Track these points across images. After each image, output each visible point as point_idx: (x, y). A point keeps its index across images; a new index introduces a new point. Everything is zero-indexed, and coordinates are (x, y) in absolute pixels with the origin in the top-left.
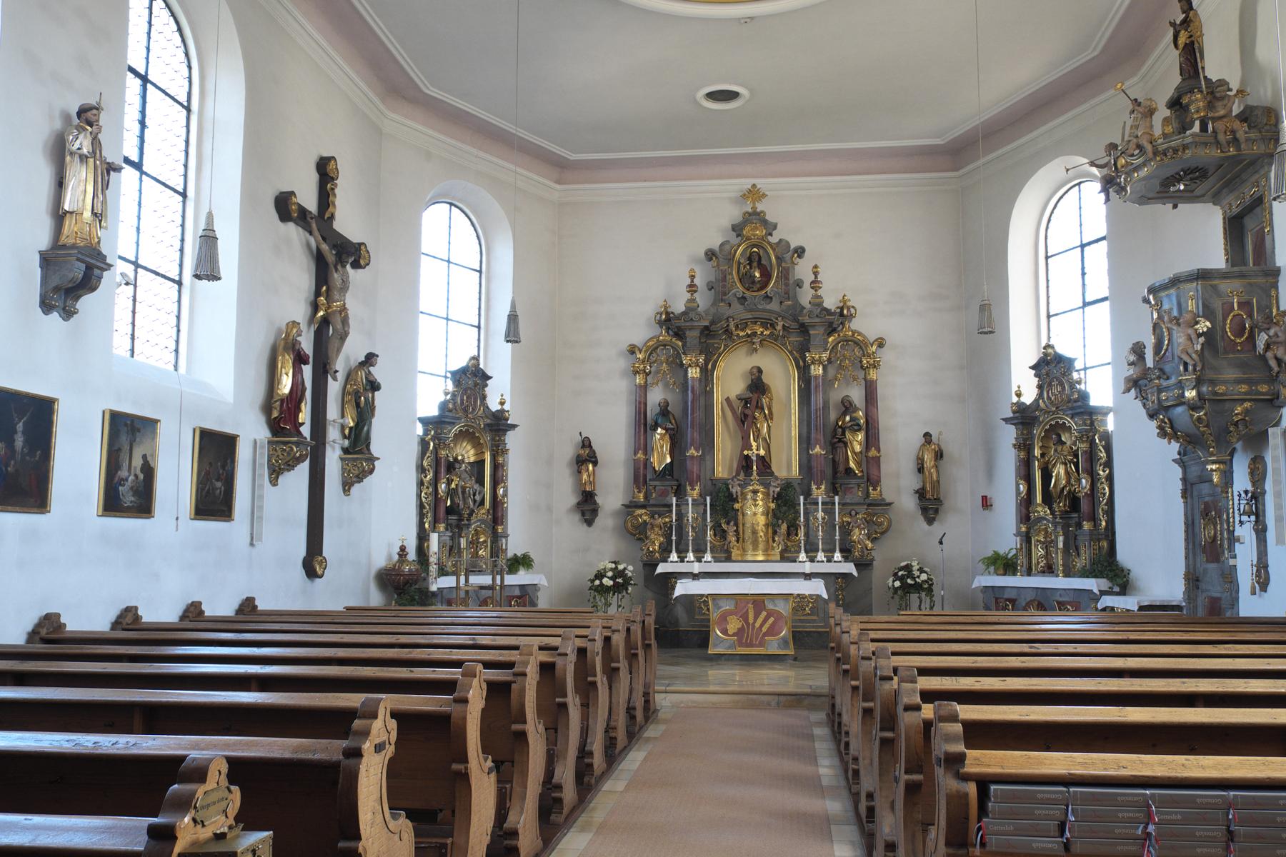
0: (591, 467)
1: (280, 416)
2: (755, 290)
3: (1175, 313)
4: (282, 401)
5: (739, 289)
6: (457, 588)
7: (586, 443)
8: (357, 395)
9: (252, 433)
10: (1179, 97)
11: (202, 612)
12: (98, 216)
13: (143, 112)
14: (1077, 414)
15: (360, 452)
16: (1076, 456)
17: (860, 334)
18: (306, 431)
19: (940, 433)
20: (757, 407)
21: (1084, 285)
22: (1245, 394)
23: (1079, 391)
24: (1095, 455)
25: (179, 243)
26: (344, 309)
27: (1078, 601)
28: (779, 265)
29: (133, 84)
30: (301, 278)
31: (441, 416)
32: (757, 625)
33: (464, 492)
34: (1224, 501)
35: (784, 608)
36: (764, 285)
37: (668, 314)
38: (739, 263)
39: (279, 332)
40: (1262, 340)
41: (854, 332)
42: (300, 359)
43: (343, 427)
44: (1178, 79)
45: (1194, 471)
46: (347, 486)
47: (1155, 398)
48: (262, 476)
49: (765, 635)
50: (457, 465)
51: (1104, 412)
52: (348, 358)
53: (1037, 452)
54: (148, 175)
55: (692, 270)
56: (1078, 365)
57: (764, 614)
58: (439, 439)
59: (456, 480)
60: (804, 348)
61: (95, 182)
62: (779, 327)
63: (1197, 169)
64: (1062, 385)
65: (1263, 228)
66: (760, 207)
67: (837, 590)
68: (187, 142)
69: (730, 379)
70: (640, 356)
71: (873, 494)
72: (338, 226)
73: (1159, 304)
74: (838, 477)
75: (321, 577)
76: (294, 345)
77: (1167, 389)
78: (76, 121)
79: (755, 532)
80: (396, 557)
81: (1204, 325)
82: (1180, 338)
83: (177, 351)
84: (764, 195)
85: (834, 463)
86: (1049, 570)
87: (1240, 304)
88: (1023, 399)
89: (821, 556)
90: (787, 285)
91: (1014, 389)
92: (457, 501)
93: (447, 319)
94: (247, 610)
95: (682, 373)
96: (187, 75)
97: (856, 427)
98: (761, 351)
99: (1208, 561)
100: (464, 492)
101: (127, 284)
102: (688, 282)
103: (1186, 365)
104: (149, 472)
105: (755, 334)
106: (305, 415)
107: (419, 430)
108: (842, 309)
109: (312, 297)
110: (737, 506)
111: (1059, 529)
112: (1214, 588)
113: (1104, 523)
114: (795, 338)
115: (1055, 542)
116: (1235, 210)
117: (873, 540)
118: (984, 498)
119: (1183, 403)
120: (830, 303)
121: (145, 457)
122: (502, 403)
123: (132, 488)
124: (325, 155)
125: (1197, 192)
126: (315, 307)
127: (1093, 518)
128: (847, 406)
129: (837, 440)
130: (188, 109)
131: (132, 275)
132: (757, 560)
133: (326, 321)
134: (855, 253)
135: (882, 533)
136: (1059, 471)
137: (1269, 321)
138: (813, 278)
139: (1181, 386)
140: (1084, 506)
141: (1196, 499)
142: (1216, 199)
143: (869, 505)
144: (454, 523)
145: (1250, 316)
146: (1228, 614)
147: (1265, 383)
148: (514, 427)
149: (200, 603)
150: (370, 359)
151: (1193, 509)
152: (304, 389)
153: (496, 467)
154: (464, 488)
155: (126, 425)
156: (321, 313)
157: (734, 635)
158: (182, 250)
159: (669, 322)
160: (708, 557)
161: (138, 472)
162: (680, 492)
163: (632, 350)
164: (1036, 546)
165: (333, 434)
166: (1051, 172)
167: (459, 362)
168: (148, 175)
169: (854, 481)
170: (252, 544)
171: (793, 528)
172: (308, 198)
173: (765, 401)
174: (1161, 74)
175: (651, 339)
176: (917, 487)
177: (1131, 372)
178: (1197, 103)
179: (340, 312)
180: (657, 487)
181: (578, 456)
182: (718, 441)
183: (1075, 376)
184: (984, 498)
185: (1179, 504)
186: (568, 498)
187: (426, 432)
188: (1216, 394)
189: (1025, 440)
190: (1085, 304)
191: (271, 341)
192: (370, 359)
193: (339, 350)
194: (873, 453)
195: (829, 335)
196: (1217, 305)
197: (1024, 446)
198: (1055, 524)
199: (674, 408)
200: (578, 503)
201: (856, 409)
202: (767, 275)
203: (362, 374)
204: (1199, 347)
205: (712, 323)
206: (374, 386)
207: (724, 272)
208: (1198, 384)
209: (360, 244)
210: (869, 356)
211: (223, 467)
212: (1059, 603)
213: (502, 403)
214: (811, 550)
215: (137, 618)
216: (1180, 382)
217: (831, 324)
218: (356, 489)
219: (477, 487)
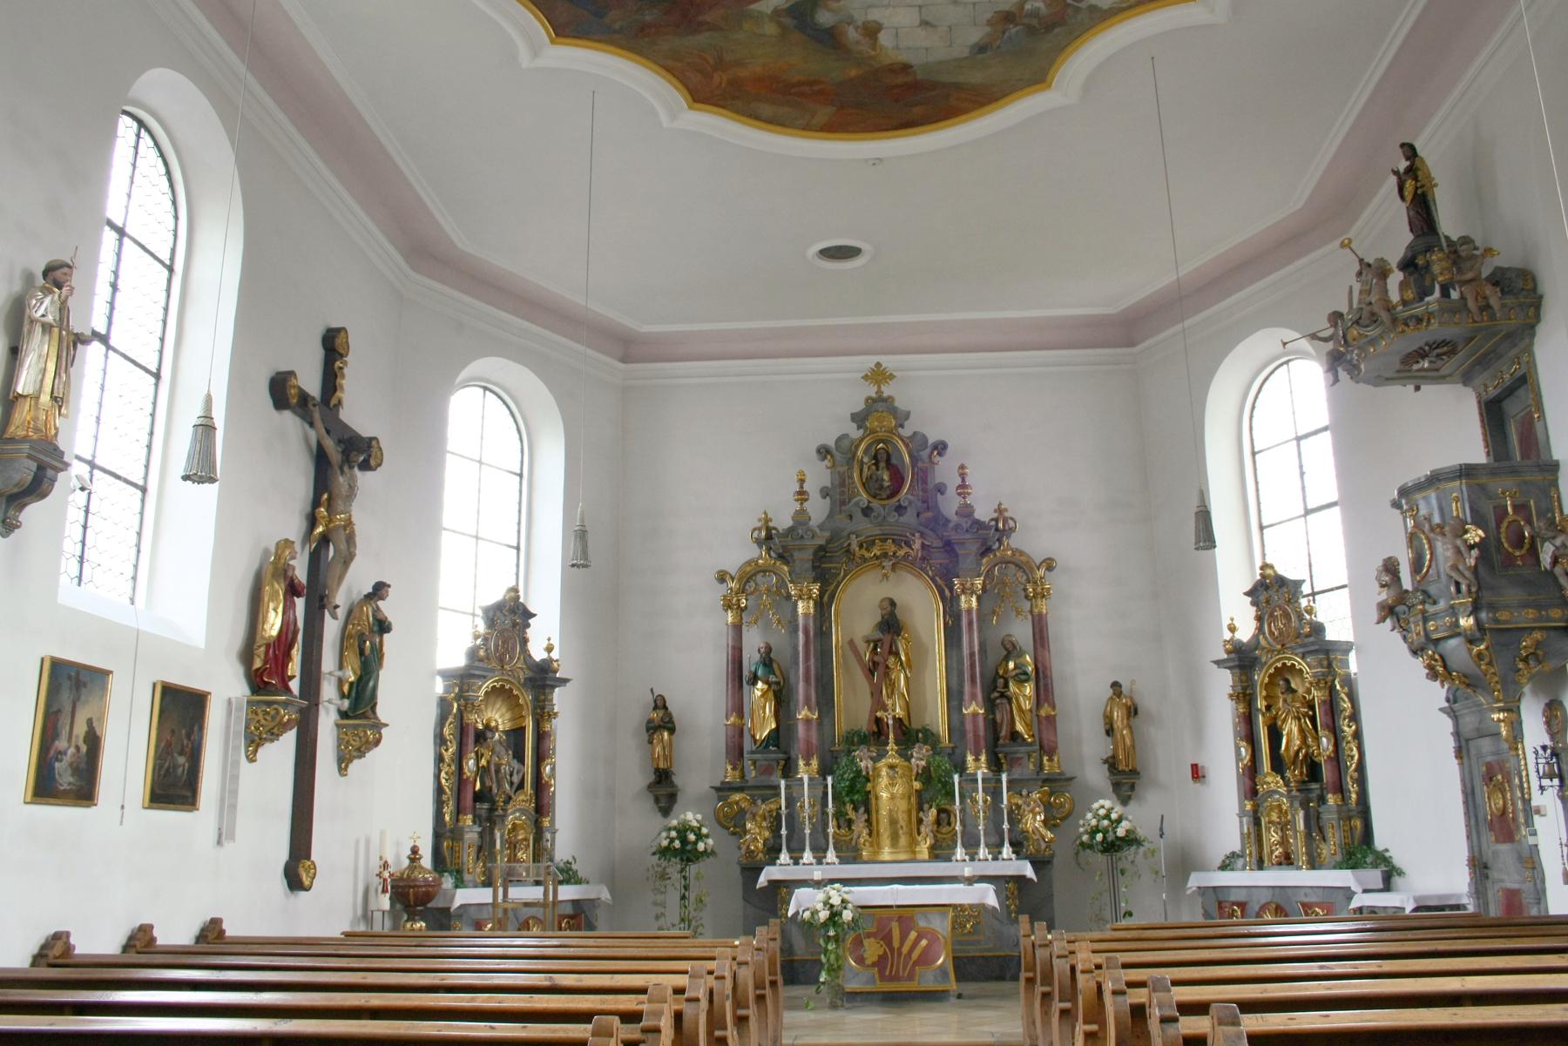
1: (265, 669)
3: (1437, 519)
4: (268, 646)
6: (494, 904)
7: (660, 704)
8: (362, 639)
9: (226, 688)
10: (1414, 257)
11: (153, 939)
12: (58, 400)
13: (116, 273)
14: (1310, 652)
15: (364, 716)
16: (1312, 708)
17: (1022, 553)
18: (294, 685)
19: (1133, 682)
21: (1303, 488)
22: (1534, 620)
23: (1311, 623)
24: (1335, 708)
25: (147, 437)
26: (349, 523)
27: (1328, 904)
29: (109, 237)
30: (300, 483)
31: (469, 667)
32: (905, 950)
34: (1513, 761)
35: (942, 926)
37: (769, 530)
39: (266, 552)
40: (1546, 558)
41: (1015, 551)
42: (293, 590)
43: (340, 682)
44: (1409, 237)
45: (1469, 722)
46: (343, 762)
47: (1420, 628)
48: (236, 748)
49: (915, 964)
50: (489, 734)
51: (1346, 648)
52: (349, 591)
53: (1261, 704)
54: (115, 351)
55: (802, 473)
56: (1306, 589)
58: (466, 699)
59: (488, 754)
61: (59, 357)
62: (917, 545)
63: (1444, 343)
64: (1286, 615)
65: (1530, 414)
66: (887, 391)
67: (1008, 898)
68: (166, 309)
72: (345, 415)
73: (1413, 509)
74: (1000, 746)
75: (307, 889)
76: (286, 571)
77: (1435, 616)
78: (40, 281)
80: (406, 862)
81: (1475, 535)
82: (1445, 551)
83: (134, 578)
84: (892, 377)
85: (993, 726)
86: (1287, 860)
87: (1515, 507)
88: (1238, 635)
89: (983, 852)
90: (925, 491)
91: (1226, 622)
92: (488, 783)
93: (477, 538)
94: (211, 936)
96: (172, 227)
97: (1022, 677)
98: (892, 576)
99: (1497, 841)
100: (498, 771)
101: (83, 489)
103: (1458, 584)
104: (94, 742)
105: (885, 555)
106: (294, 667)
108: (997, 520)
109: (309, 509)
111: (1297, 804)
112: (1507, 876)
113: (1354, 796)
114: (939, 559)
115: (1294, 822)
116: (1492, 392)
118: (1195, 767)
119: (1459, 634)
120: (983, 513)
121: (90, 722)
122: (549, 649)
123: (71, 765)
124: (335, 325)
125: (1442, 372)
126: (312, 521)
127: (1340, 789)
128: (1011, 650)
129: (996, 691)
130: (171, 269)
131: (87, 476)
132: (889, 859)
133: (325, 539)
134: (1012, 454)
135: (1062, 819)
136: (1290, 729)
137: (1555, 529)
138: (959, 481)
139: (1453, 611)
140: (1326, 773)
141: (1474, 759)
142: (1466, 379)
144: (484, 814)
145: (1529, 522)
146: (1534, 912)
147: (1557, 606)
149: (151, 927)
150: (379, 590)
151: (1471, 772)
152: (296, 632)
153: (541, 737)
155: (70, 678)
156: (320, 529)
157: (874, 965)
158: (149, 447)
160: (831, 855)
161: (81, 743)
162: (788, 770)
164: (1268, 830)
165: (328, 691)
167: (496, 595)
168: (115, 351)
169: (1023, 749)
170: (219, 842)
171: (944, 817)
172: (310, 381)
174: (1386, 230)
177: (1384, 595)
178: (1438, 264)
179: (345, 528)
180: (763, 761)
181: (650, 721)
183: (1304, 602)
184: (1195, 767)
185: (1453, 767)
186: (636, 777)
188: (1497, 621)
189: (1244, 689)
190: (1308, 512)
191: (256, 566)
192: (379, 590)
193: (341, 578)
195: (983, 554)
196: (1488, 509)
197: (1244, 696)
200: (650, 787)
201: (1021, 654)
202: (898, 479)
203: (368, 610)
204: (1473, 562)
205: (829, 541)
206: (383, 626)
208: (1475, 610)
209: (371, 439)
211: (189, 736)
212: (1304, 905)
213: (549, 649)
214: (971, 845)
215: (69, 949)
216: (1452, 607)
217: (985, 541)
218: (356, 766)
219: (515, 764)
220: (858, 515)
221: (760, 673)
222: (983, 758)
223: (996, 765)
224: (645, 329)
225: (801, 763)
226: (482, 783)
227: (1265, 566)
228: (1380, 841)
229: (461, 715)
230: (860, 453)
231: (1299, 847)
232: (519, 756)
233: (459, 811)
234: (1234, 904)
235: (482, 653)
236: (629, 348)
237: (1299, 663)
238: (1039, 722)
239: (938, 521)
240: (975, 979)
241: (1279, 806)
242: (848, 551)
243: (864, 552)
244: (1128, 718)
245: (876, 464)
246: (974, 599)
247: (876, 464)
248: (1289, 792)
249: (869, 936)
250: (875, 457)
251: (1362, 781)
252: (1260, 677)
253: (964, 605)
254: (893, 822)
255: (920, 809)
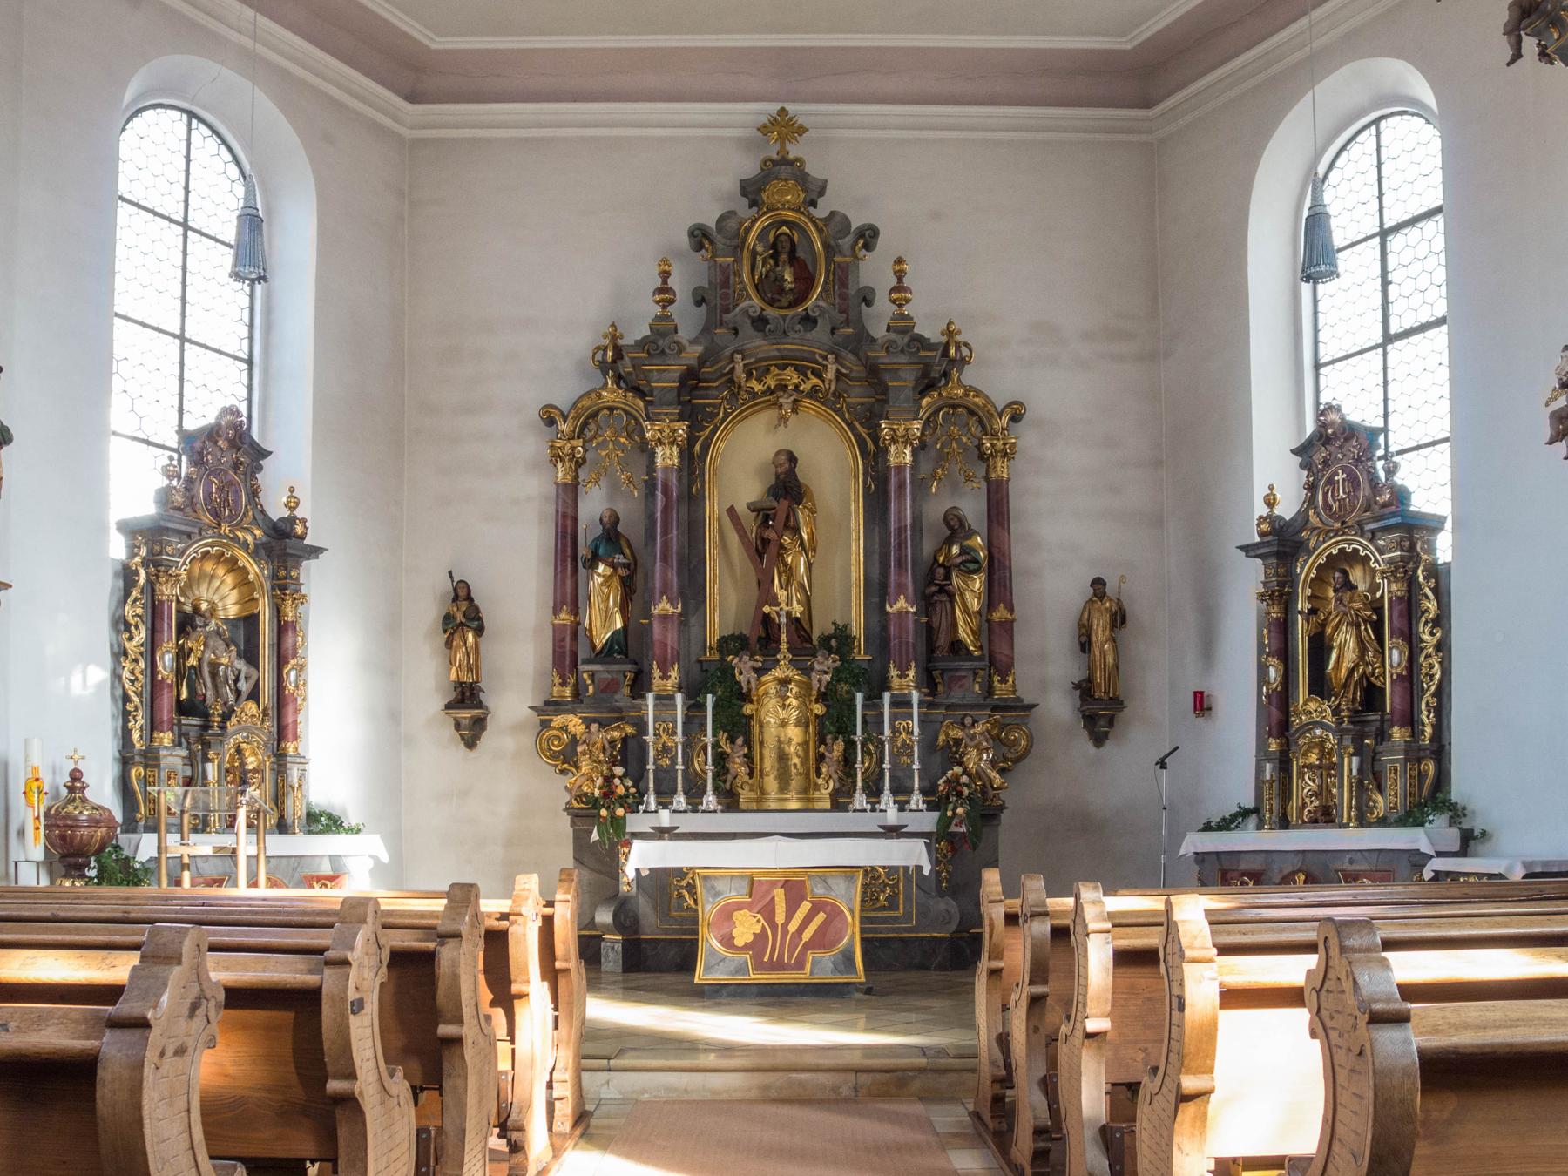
0: (470, 637)
2: (780, 292)
5: (755, 303)
7: (462, 593)
14: (1386, 529)
16: (1378, 610)
17: (978, 393)
19: (1122, 579)
20: (786, 526)
28: (829, 260)
33: (214, 674)
35: (848, 899)
36: (801, 296)
38: (754, 254)
41: (968, 390)
49: (807, 946)
50: (199, 621)
51: (1432, 525)
57: (806, 907)
58: (157, 564)
60: (871, 419)
62: (830, 374)
66: (793, 151)
69: (742, 459)
70: (565, 427)
71: (1001, 690)
74: (938, 659)
79: (783, 757)
84: (802, 130)
85: (930, 632)
86: (1326, 816)
88: (1277, 511)
90: (844, 297)
91: (1259, 492)
92: (200, 689)
95: (644, 461)
97: (969, 565)
100: (214, 674)
102: (658, 283)
105: (783, 387)
107: (118, 549)
110: (748, 709)
111: (1347, 741)
113: (1428, 730)
114: (858, 396)
117: (1002, 772)
120: (930, 330)
128: (955, 528)
129: (935, 590)
134: (976, 247)
135: (1017, 761)
138: (894, 282)
140: (1392, 699)
143: (995, 709)
144: (193, 733)
148: (315, 551)
153: (283, 629)
154: (214, 666)
157: (747, 947)
159: (617, 362)
163: (549, 418)
164: (1301, 775)
166: (1336, 89)
169: (967, 664)
173: (802, 516)
175: (587, 394)
176: (1078, 675)
182: (713, 589)
187: (132, 550)
189: (1281, 584)
190: (1389, 338)
194: (1000, 614)
195: (923, 392)
197: (1280, 594)
198: (1340, 732)
199: (631, 527)
200: (448, 707)
201: (970, 534)
202: (806, 280)
205: (703, 360)
207: (724, 269)
210: (995, 435)
213: (293, 504)
219: (241, 665)
220: (747, 329)
221: (601, 551)
222: (911, 673)
223: (929, 682)
224: (439, 43)
225: (656, 673)
226: (191, 689)
227: (1320, 413)
228: (1461, 787)
229: (151, 586)
230: (751, 239)
231: (1345, 797)
232: (251, 656)
233: (154, 725)
234: (1244, 874)
235: (179, 499)
236: (416, 76)
237: (1363, 546)
238: (990, 630)
239: (862, 339)
240: (889, 968)
241: (1322, 744)
242: (731, 381)
243: (754, 384)
244: (1112, 629)
245: (775, 256)
246: (908, 451)
247: (775, 256)
248: (1340, 722)
249: (740, 906)
250: (774, 246)
251: (1441, 711)
252: (1306, 569)
253: (893, 461)
254: (783, 757)
255: (822, 740)
